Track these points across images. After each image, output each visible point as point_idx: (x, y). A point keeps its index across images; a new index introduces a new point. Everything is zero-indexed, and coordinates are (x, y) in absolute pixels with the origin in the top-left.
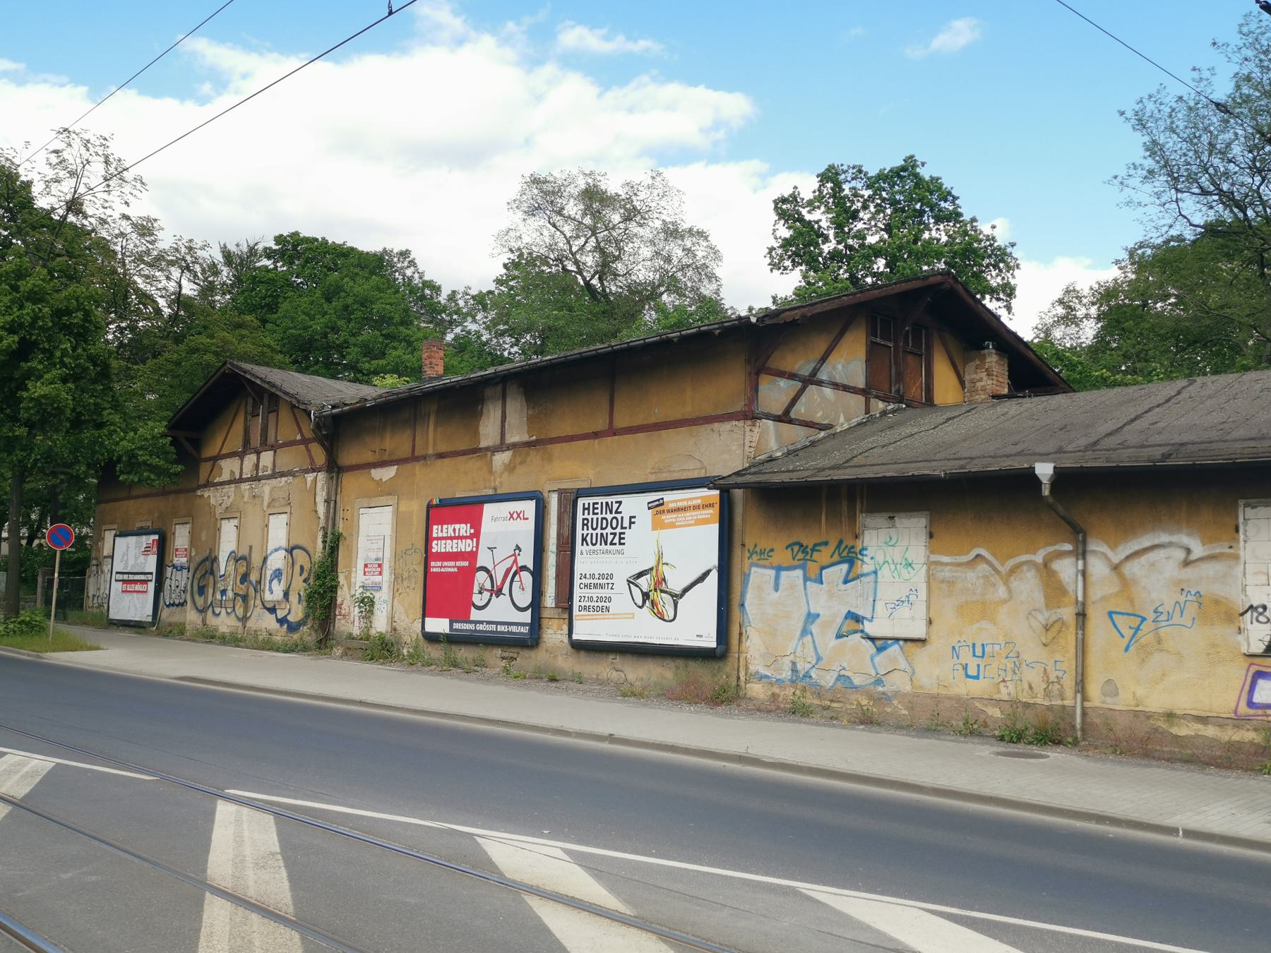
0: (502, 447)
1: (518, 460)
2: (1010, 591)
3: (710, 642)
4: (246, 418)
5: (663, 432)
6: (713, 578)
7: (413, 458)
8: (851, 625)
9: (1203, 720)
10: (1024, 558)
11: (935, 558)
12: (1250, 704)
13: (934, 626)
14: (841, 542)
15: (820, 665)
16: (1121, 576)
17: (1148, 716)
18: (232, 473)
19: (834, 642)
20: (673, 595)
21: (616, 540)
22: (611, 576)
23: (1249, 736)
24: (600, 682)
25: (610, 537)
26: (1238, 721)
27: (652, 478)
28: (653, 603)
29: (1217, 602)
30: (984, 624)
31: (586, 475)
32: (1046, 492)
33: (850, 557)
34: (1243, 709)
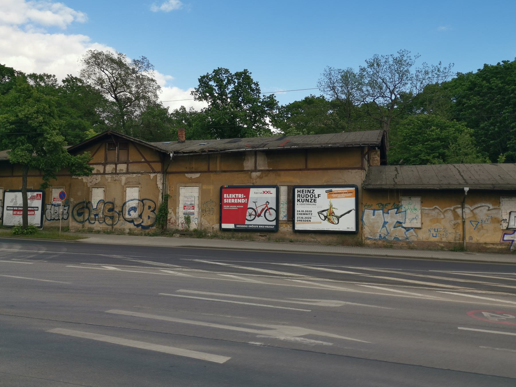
0: (256, 170)
1: (264, 175)
2: (444, 216)
3: (354, 229)
4: (106, 152)
5: (329, 171)
6: (353, 213)
7: (209, 171)
8: (398, 224)
9: (493, 244)
10: (448, 208)
11: (423, 208)
12: (503, 240)
13: (423, 225)
14: (394, 203)
15: (389, 235)
16: (473, 213)
17: (480, 244)
18: (98, 170)
19: (393, 229)
20: (337, 217)
21: (313, 201)
22: (311, 211)
23: (504, 247)
24: (309, 242)
25: (310, 200)
26: (501, 244)
27: (325, 184)
28: (329, 219)
29: (496, 218)
30: (438, 224)
31: (297, 181)
32: (466, 194)
33: (398, 207)
34: (502, 241)
